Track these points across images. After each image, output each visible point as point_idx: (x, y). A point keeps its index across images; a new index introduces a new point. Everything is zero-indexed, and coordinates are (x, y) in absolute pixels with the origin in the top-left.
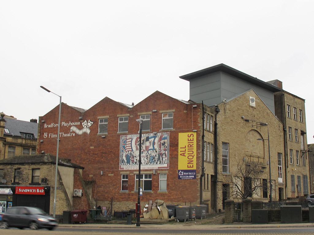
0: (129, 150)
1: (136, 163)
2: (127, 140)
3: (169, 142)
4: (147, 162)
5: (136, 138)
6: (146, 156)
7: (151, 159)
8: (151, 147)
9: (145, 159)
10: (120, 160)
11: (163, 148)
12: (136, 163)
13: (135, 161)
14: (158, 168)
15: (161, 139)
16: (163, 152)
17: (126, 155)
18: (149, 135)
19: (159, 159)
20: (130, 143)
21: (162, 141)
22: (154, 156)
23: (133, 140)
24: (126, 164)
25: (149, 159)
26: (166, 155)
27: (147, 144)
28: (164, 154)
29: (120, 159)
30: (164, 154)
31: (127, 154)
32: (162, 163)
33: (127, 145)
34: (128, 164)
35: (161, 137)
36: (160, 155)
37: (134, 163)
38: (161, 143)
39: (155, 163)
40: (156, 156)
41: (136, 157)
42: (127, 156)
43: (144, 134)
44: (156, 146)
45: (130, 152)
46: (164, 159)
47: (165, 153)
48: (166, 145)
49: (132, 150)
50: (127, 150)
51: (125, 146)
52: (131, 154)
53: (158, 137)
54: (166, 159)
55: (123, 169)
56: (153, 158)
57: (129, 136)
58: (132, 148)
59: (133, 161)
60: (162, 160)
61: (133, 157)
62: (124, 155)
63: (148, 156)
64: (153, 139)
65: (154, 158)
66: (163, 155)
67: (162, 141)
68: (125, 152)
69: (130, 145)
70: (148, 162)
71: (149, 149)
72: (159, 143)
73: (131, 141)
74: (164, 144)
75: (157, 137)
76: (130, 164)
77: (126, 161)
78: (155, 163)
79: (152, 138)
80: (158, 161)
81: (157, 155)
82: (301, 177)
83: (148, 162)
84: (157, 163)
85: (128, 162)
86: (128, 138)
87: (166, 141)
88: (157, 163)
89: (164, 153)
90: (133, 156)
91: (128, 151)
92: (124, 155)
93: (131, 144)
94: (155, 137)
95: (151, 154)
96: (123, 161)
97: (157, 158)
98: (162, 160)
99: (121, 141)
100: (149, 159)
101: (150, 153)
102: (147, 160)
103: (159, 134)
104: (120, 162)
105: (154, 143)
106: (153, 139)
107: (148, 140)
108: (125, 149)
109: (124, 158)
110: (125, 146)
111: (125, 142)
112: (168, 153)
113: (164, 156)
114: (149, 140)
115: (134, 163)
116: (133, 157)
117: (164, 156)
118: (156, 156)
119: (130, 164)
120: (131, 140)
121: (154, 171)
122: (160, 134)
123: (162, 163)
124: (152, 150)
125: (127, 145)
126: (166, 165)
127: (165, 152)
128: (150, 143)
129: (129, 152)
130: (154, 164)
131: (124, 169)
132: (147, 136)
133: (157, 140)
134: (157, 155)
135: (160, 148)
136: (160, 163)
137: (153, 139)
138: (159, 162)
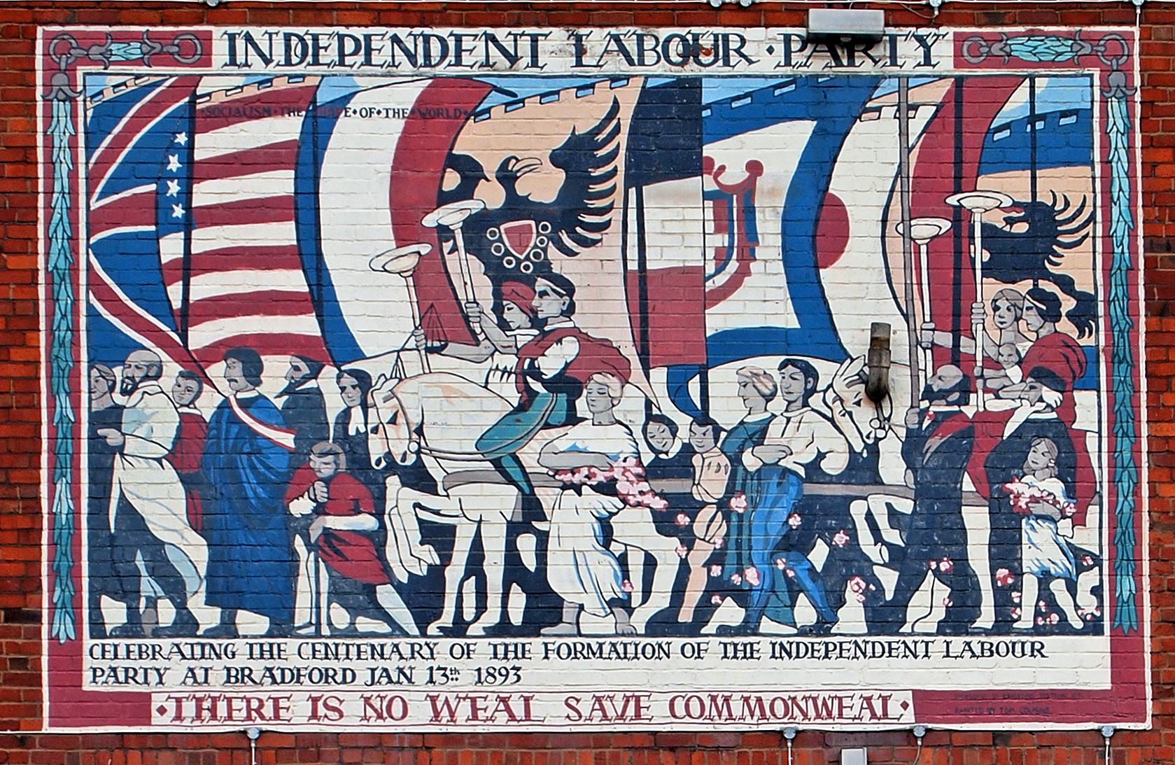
0: (278, 343)
1: (424, 596)
2: (198, 119)
3: (1130, 222)
4: (665, 579)
5: (408, 95)
6: (656, 470)
7: (762, 538)
8: (763, 300)
9: (636, 529)
10: (66, 541)
11: (1001, 319)
12: (424, 596)
13: (408, 555)
14: (925, 701)
15: (955, 148)
16: (1023, 405)
17: (189, 424)
18: (692, 51)
19: (929, 538)
20: (280, 183)
21: (994, 197)
22: (814, 468)
23: (345, 130)
24: (208, 617)
25: (710, 530)
26: (1071, 466)
27: (676, 225)
28: (1041, 453)
29: (58, 499)
30: (1041, 453)
31: (207, 406)
32: (1004, 624)
33: (207, 239)
34: (252, 623)
35: (963, 103)
36: (960, 453)
37: (387, 597)
38: (960, 217)
39: (852, 616)
40: (864, 468)
41: (418, 478)
42: (203, 453)
43: (596, 38)
44: (860, 290)
45: (277, 371)
46: (1040, 547)
47: (1062, 432)
48: (1079, 265)
49: (336, 345)
50: (202, 336)
51: (171, 248)
52: (303, 408)
53: (906, 110)
54: (1089, 538)
55: (139, 707)
56: (804, 507)
57: (235, 60)
58: (320, 298)
59: (358, 571)
60: (1005, 548)
61: (363, 480)
62: (155, 418)
63: (682, 465)
64: (802, 130)
65: (823, 515)
66: (1008, 459)
67: (994, 197)
68: (173, 369)
69: (280, 183)
70: (693, 596)
71: (718, 320)
72: (924, 229)
73: (306, 158)
74: (1027, 247)
75: (886, 98)
76: (283, 625)
77: (192, 553)
78: (852, 616)
79: (763, 109)
80: (908, 587)
81: (892, 467)
82: (202, 596)
83: (693, 596)
84: (886, 617)
85: (250, 579)
86: (216, 85)
87: (1066, 185)
88: (886, 617)
89: (1032, 429)
90: (355, 448)
91: (247, 354)
92: (155, 418)
93: (303, 208)
94: (831, 111)
95: (758, 435)
96: (123, 551)
97: (879, 512)
98: (1005, 548)
99: (58, 131)
100: (710, 530)
101: (728, 408)
102: (668, 550)
103: (909, 51)
104: (66, 574)
105: (816, 228)
106: (782, 146)
107: (690, 164)
108: (160, 305)
109: (156, 495)
110: (171, 248)
111: (145, 165)
112: (1119, 422)
113: (1038, 483)
114: (697, 166)
115: (387, 597)
116: (363, 480)
117: (1038, 483)
118: (864, 468)
119: (283, 625)
120: (288, 128)
121: (367, 522)
122: (944, 52)
123: (1004, 624)
124: (770, 363)
125: (207, 239)
126: (1082, 664)
127: (1067, 409)
128: (734, 208)
129: (254, 374)
130: (823, 627)
131: (160, 724)
132: (659, 71)
133: (870, 164)
134: (892, 467)
135: (955, 315)
136: (958, 620)
137: (782, 146)
138: (931, 601)
